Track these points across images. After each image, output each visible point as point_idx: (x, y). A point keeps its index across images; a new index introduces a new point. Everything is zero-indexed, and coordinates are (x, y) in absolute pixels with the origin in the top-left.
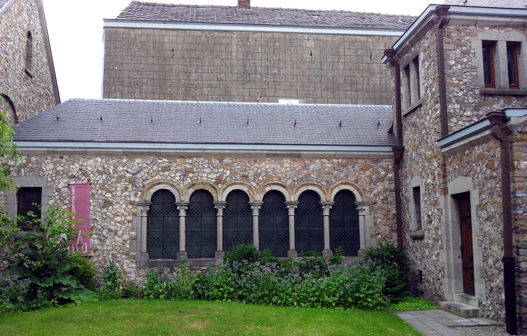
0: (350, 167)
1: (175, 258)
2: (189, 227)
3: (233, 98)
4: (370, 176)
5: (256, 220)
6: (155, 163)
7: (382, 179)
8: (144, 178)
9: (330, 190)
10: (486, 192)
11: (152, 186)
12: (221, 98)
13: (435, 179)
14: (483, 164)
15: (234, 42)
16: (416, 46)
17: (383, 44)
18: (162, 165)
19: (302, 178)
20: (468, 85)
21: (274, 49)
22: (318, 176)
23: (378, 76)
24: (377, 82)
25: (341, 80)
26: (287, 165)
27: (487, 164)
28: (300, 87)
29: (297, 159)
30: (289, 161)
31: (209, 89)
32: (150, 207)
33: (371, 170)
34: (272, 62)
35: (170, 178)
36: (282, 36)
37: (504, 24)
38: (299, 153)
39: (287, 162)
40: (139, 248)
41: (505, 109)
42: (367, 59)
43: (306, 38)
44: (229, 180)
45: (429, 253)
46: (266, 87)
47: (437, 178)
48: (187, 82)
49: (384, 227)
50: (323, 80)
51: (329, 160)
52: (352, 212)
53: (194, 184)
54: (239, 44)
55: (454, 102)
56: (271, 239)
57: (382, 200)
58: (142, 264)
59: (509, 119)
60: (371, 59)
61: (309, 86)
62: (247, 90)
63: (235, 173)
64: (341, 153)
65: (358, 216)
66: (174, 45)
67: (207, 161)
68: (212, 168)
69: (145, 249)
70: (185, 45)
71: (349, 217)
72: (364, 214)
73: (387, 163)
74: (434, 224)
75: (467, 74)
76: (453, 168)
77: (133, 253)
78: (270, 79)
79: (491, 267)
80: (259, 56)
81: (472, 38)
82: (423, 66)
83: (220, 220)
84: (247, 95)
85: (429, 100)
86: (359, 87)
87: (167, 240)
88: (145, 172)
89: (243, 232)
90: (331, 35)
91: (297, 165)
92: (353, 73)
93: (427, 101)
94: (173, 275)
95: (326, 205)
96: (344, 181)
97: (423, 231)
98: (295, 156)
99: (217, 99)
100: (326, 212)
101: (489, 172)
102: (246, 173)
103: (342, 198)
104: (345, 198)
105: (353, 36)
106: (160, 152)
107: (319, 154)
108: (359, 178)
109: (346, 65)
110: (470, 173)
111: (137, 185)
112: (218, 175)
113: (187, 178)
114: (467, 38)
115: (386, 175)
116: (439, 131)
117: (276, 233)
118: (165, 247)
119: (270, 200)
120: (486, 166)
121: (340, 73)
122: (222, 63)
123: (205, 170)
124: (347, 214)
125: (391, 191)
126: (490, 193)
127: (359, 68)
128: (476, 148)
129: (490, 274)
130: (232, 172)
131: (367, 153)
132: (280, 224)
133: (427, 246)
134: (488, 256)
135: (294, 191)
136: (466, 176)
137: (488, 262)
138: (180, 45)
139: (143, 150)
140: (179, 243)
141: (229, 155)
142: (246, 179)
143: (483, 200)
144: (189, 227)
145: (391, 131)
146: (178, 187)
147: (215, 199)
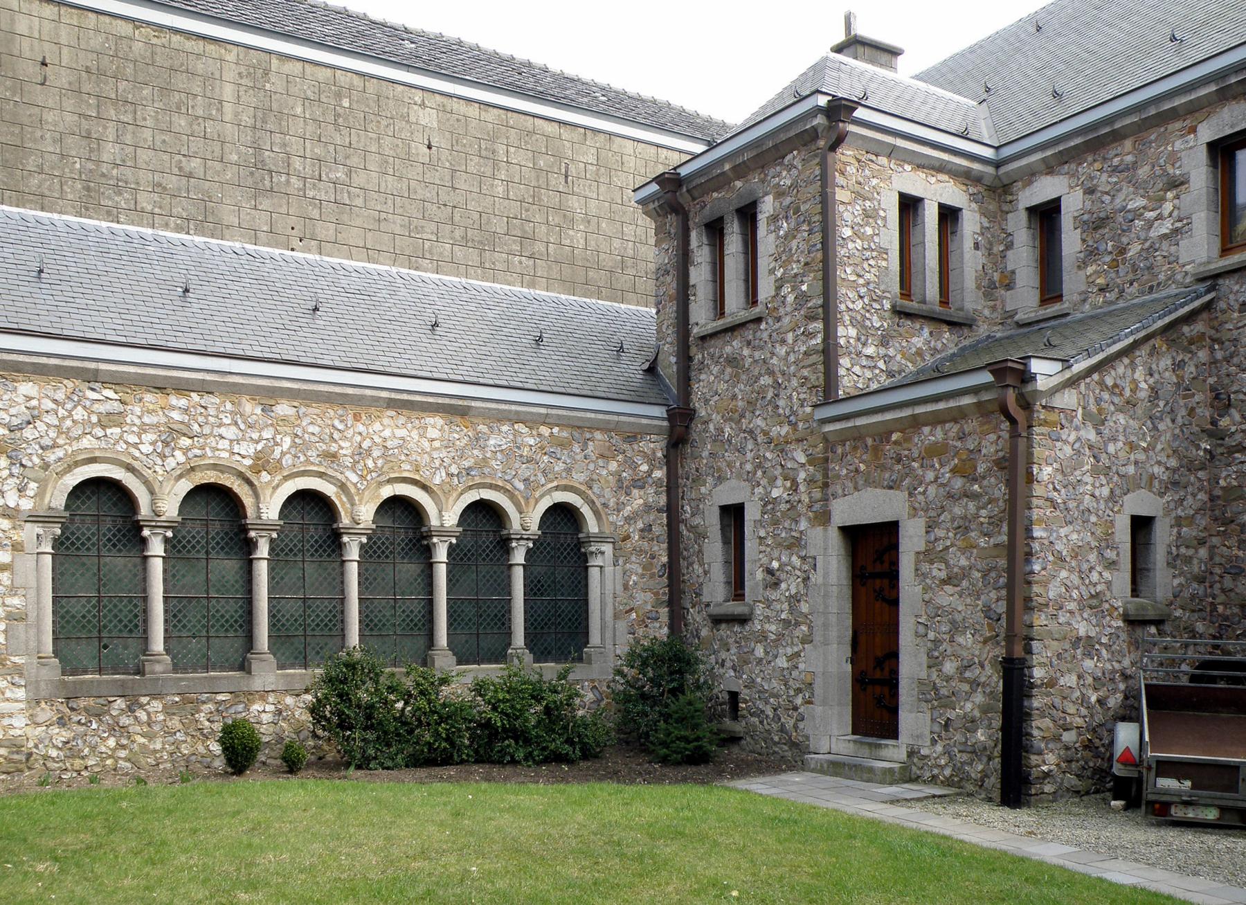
0: (577, 448)
1: (140, 671)
2: (174, 586)
3: (226, 231)
4: (618, 474)
5: (353, 570)
6: (79, 401)
7: (639, 483)
8: (46, 441)
9: (532, 501)
10: (944, 525)
11: (69, 466)
12: (192, 226)
13: (795, 490)
14: (942, 465)
15: (230, 75)
16: (750, 177)
17: (593, 151)
18: (98, 407)
19: (470, 468)
20: (871, 286)
21: (337, 115)
22: (507, 464)
23: (582, 227)
24: (578, 241)
25: (499, 226)
26: (433, 433)
28: (401, 226)
29: (458, 419)
30: (438, 421)
31: (156, 197)
32: (64, 528)
33: (620, 458)
34: (331, 148)
35: (125, 446)
36: (357, 81)
37: (937, 164)
38: (466, 403)
39: (434, 427)
40: (33, 644)
41: (1030, 357)
42: (557, 181)
43: (418, 99)
44: (290, 462)
45: (767, 653)
46: (315, 213)
47: (802, 488)
48: (91, 166)
49: (642, 594)
50: (457, 218)
51: (531, 428)
52: (572, 558)
53: (193, 469)
54: (243, 81)
55: (848, 322)
56: (388, 620)
57: (642, 530)
58: (44, 690)
59: (1033, 378)
60: (566, 182)
61: (422, 227)
62: (265, 216)
63: (307, 446)
64: (560, 412)
65: (587, 568)
66: (47, 46)
67: (229, 406)
68: (242, 426)
69: (48, 647)
70: (81, 55)
72: (601, 564)
73: (652, 445)
75: (872, 262)
76: (851, 468)
77: (16, 659)
78: (324, 192)
79: (948, 679)
80: (297, 127)
81: (882, 185)
82: (773, 228)
83: (262, 570)
84: (265, 229)
85: (789, 309)
86: (539, 247)
87: (110, 621)
88: (48, 425)
89: (318, 602)
90: (477, 105)
91: (460, 435)
92: (527, 210)
93: (782, 311)
94: (136, 718)
95: (522, 539)
96: (564, 482)
97: (749, 605)
98: (456, 411)
99: (178, 229)
100: (519, 557)
101: (958, 483)
102: (334, 447)
103: (552, 524)
104: (559, 523)
105: (528, 117)
106: (97, 370)
107: (510, 411)
108: (595, 477)
109: (323, 168)
110: (902, 481)
111: (24, 462)
112: (259, 447)
113: (173, 449)
114: (874, 182)
115: (649, 473)
116: (817, 384)
117: (400, 607)
118: (105, 641)
119: (89, 507)
120: (951, 471)
121: (497, 206)
122: (195, 127)
123: (223, 431)
125: (659, 511)
126: (960, 527)
127: (540, 200)
129: (946, 693)
130: (297, 440)
131: (615, 418)
132: (411, 583)
133: (763, 637)
134: (944, 655)
135: (451, 500)
136: (891, 488)
137: (944, 670)
138: (65, 51)
139: (44, 360)
140: (145, 631)
141: (291, 394)
142: (332, 462)
144: (174, 586)
145: (651, 370)
146: (147, 473)
147: (250, 512)
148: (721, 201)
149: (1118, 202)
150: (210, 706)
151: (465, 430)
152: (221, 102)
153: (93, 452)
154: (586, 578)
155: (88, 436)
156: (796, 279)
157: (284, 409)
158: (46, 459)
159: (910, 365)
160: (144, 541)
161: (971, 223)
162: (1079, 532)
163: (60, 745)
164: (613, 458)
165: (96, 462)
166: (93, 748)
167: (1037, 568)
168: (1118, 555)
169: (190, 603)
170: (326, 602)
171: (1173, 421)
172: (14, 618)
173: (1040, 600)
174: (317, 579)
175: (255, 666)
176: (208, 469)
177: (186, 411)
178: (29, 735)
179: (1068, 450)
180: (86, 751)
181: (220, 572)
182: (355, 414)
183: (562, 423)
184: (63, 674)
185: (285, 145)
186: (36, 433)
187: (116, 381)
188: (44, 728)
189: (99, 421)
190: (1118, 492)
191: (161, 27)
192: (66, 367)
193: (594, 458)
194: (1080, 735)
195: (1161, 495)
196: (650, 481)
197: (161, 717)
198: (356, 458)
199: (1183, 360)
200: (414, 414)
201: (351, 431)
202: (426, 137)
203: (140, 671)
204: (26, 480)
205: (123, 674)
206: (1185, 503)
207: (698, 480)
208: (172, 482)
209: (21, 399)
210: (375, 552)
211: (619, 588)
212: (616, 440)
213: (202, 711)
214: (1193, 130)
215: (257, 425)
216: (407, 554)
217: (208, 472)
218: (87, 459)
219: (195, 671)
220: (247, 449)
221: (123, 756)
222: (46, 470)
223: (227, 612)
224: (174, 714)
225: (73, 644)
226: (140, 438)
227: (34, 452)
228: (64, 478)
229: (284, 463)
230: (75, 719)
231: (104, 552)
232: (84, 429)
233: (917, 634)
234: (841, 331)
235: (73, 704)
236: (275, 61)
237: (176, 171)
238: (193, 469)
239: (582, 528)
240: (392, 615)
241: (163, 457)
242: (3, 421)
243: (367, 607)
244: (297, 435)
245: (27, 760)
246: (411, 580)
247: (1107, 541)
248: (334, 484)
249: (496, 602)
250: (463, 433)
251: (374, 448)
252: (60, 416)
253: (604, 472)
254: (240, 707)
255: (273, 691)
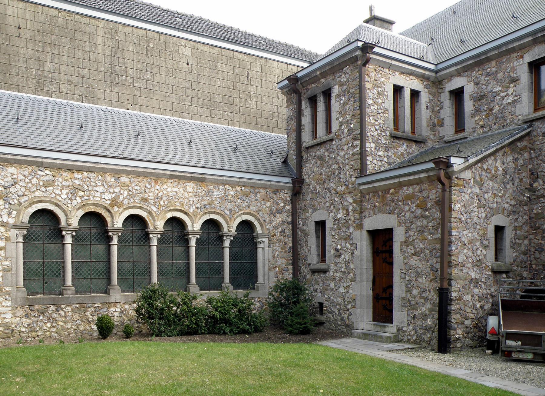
0: (252, 196)
1: (61, 294)
2: (76, 256)
3: (99, 101)
4: (270, 208)
5: (154, 250)
6: (35, 175)
7: (280, 211)
8: (20, 193)
9: (233, 219)
10: (413, 230)
11: (30, 204)
12: (84, 99)
13: (348, 215)
14: (412, 204)
15: (101, 33)
16: (328, 77)
18: (43, 178)
19: (205, 205)
20: (381, 125)
21: (147, 51)
22: (222, 203)
23: (254, 99)
24: (253, 105)
25: (218, 99)
26: (189, 189)
27: (418, 204)
28: (175, 99)
29: (200, 184)
30: (192, 184)
31: (68, 86)
32: (28, 231)
33: (271, 200)
34: (145, 65)
35: (54, 195)
36: (156, 35)
37: (410, 72)
38: (204, 176)
39: (190, 187)
40: (14, 282)
41: (450, 156)
42: (244, 79)
43: (183, 43)
44: (127, 202)
45: (335, 286)
46: (138, 93)
47: (351, 214)
48: (40, 72)
49: (281, 260)
50: (200, 95)
51: (232, 187)
53: (84, 205)
54: (106, 36)
55: (371, 141)
56: (170, 271)
57: (281, 232)
58: (19, 302)
59: (452, 165)
60: (248, 80)
61: (185, 99)
62: (116, 95)
63: (134, 195)
64: (245, 180)
65: (257, 248)
66: (20, 20)
67: (100, 178)
68: (106, 186)
69: (21, 283)
70: (36, 24)
71: (247, 249)
72: (263, 247)
73: (285, 195)
74: (345, 258)
75: (381, 115)
77: (7, 289)
78: (142, 84)
79: (415, 297)
80: (130, 56)
81: (386, 81)
82: (338, 100)
83: (115, 250)
84: (116, 100)
85: (345, 135)
86: (236, 108)
87: (48, 272)
88: (21, 186)
89: (139, 264)
90: (209, 46)
91: (201, 190)
92: (231, 92)
94: (59, 314)
95: (228, 236)
96: (247, 211)
97: (328, 265)
98: (199, 180)
99: (78, 100)
100: (227, 244)
102: (146, 196)
103: (241, 229)
104: (244, 229)
105: (231, 51)
106: (42, 162)
107: (223, 180)
108: (260, 209)
109: (141, 73)
110: (394, 211)
111: (10, 202)
112: (113, 196)
113: (76, 197)
114: (382, 79)
115: (284, 207)
116: (357, 168)
117: (175, 266)
118: (46, 280)
119: (39, 222)
120: (416, 206)
121: (218, 90)
122: (85, 56)
123: (97, 188)
124: (246, 246)
125: (288, 223)
126: (420, 231)
127: (236, 87)
128: (405, 188)
130: (130, 193)
131: (269, 183)
132: (180, 255)
133: (334, 279)
134: (413, 286)
135: (197, 219)
136: (390, 213)
137: (413, 293)
138: (28, 22)
139: (19, 158)
140: (64, 276)
141: (127, 173)
142: (145, 202)
143: (409, 236)
144: (76, 256)
146: (64, 207)
147: (109, 224)
148: (315, 88)
149: (489, 88)
150: (92, 309)
151: (204, 188)
152: (96, 45)
153: (41, 198)
154: (256, 253)
155: (39, 191)
156: (348, 122)
157: (124, 179)
158: (20, 201)
159: (398, 160)
160: (63, 237)
161: (425, 98)
162: (472, 233)
163: (26, 326)
164: (268, 200)
165: (42, 202)
166: (41, 327)
167: (453, 248)
168: (489, 243)
169: (83, 264)
170: (143, 264)
171: (513, 184)
172: (6, 270)
173: (455, 263)
174: (139, 253)
175: (111, 291)
176: (91, 205)
177: (81, 180)
178: (13, 322)
179: (467, 197)
180: (38, 329)
181: (96, 250)
182: (155, 181)
183: (246, 185)
184: (28, 295)
185: (125, 63)
186: (16, 189)
187: (51, 167)
188: (19, 319)
189: (43, 184)
190: (489, 215)
191: (70, 12)
192: (29, 160)
193: (260, 201)
194: (472, 321)
195: (508, 216)
196: (284, 210)
197: (70, 314)
198: (156, 200)
199: (517, 158)
200: (181, 181)
201: (153, 189)
202: (186, 60)
203: (61, 294)
204: (11, 210)
205: (54, 295)
206: (518, 220)
207: (305, 210)
208: (75, 211)
209: (9, 175)
210: (164, 242)
211: (271, 257)
212: (270, 192)
213: (88, 311)
214: (522, 57)
215: (112, 186)
216: (178, 242)
217: (91, 207)
218: (38, 201)
219: (85, 294)
220: (108, 196)
221: (54, 331)
222: (20, 206)
223: (99, 268)
224: (76, 312)
225: (32, 282)
226: (61, 192)
227: (15, 198)
228: (28, 209)
229: (124, 202)
230: (33, 314)
231: (45, 242)
232: (37, 188)
233: (401, 278)
234: (368, 145)
235: (32, 308)
236: (120, 27)
237: (77, 75)
238: (84, 205)
239: (254, 231)
240: (171, 269)
241: (71, 200)
242: (1, 184)
243: (161, 266)
244: (130, 190)
245: (12, 332)
246: (180, 254)
247: (484, 237)
248: (146, 212)
249: (217, 263)
250: (202, 190)
251: (164, 196)
252: (26, 182)
253: (264, 207)
254: (105, 309)
255: (119, 302)
